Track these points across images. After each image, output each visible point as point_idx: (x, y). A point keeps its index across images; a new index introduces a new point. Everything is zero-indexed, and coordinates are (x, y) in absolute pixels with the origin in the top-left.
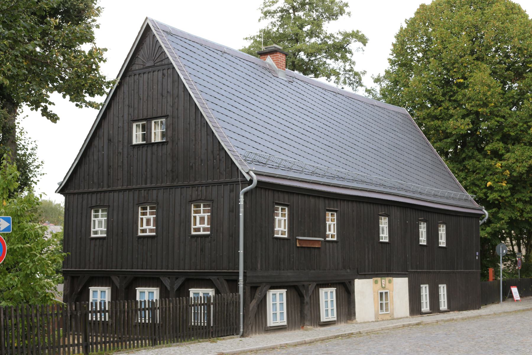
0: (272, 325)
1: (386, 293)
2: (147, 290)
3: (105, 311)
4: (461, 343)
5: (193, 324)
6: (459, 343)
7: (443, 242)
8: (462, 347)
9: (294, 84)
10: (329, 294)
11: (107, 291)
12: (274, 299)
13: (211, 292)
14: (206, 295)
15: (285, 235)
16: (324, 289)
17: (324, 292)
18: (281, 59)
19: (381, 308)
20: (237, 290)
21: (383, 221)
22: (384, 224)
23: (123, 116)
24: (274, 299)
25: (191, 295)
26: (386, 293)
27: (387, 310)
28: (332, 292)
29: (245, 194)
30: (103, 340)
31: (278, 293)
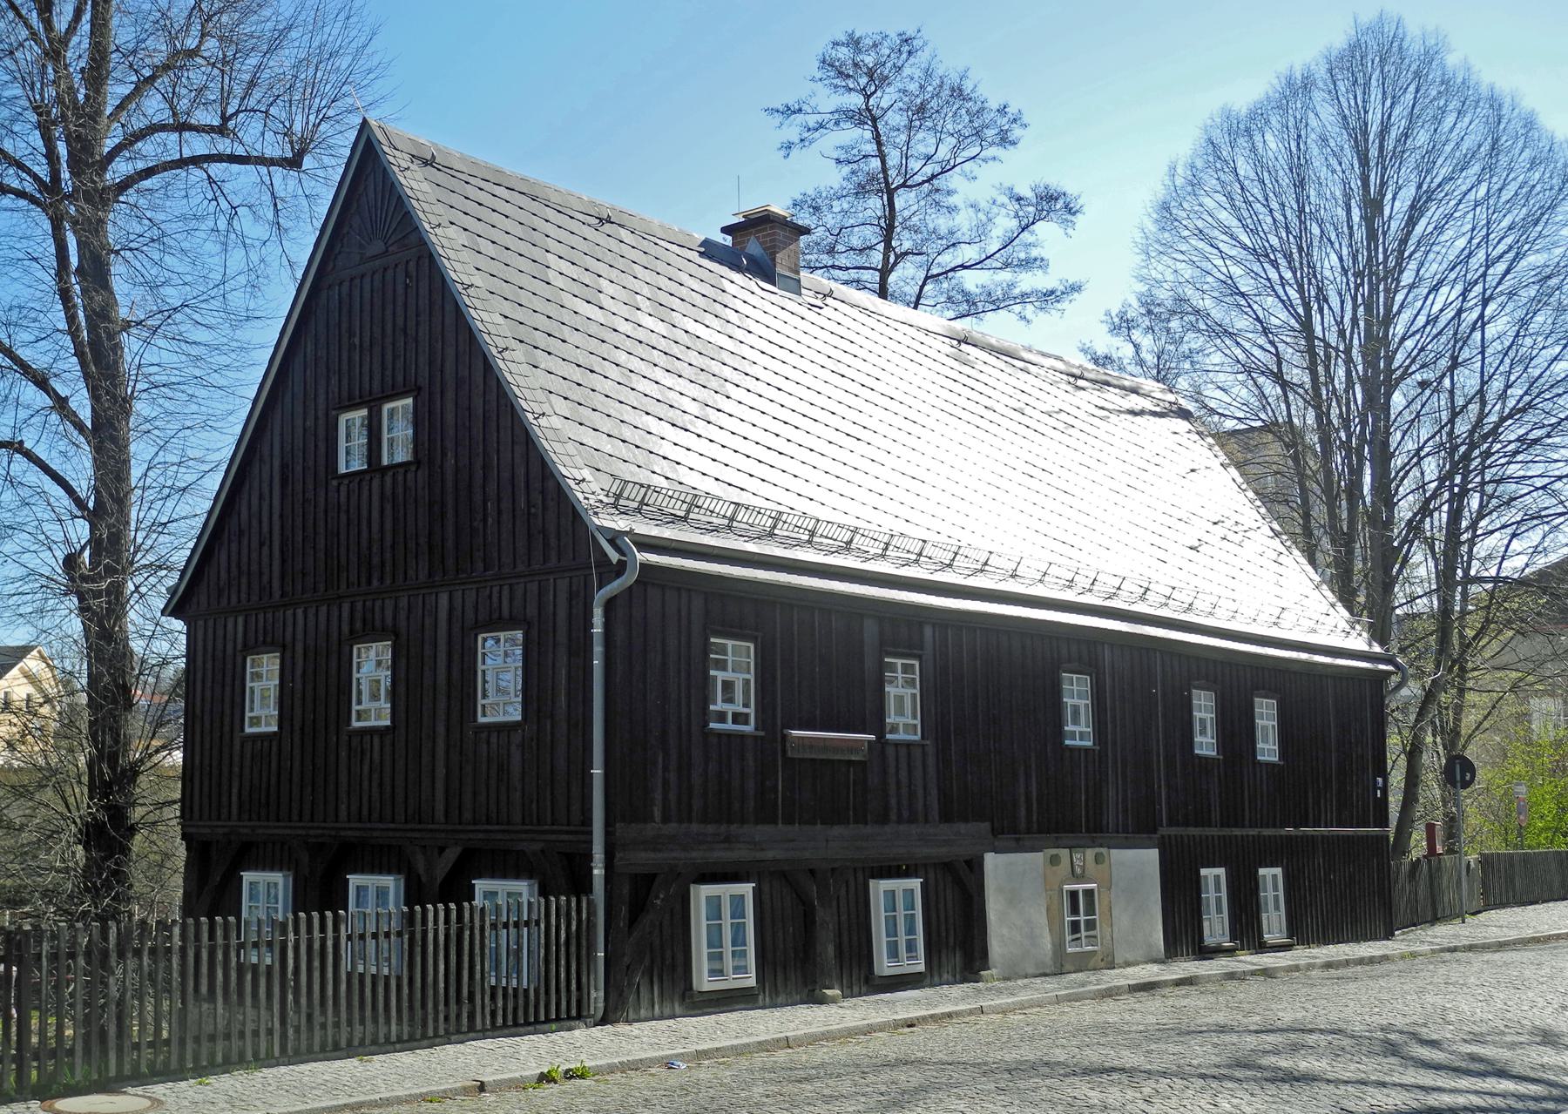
0: (887, 972)
7: (1268, 749)
9: (826, 311)
15: (746, 723)
23: (667, 478)
26: (1089, 894)
29: (609, 605)
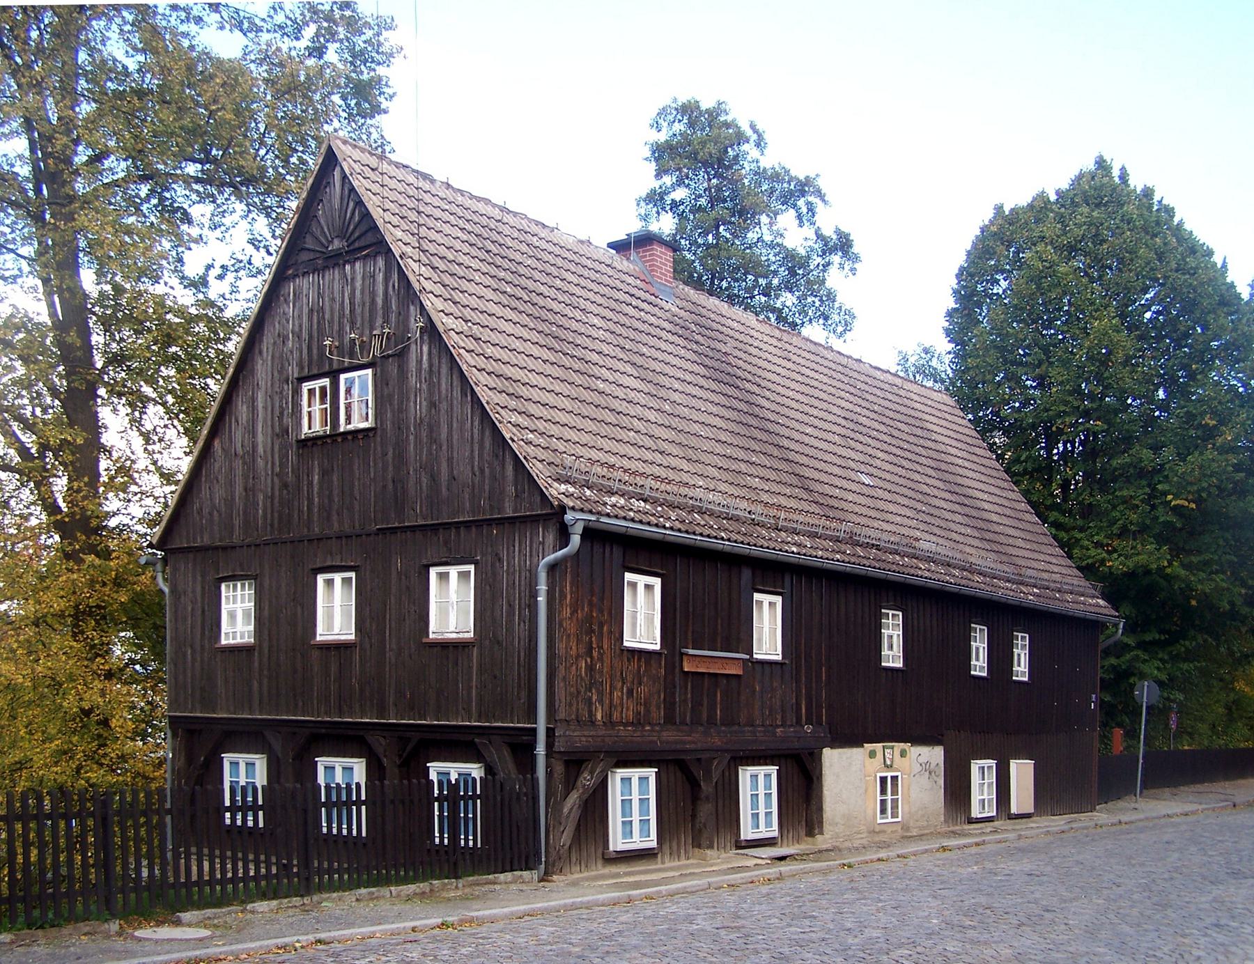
0: (620, 847)
1: (895, 778)
2: (338, 763)
3: (255, 808)
4: (1071, 900)
5: (437, 840)
6: (1065, 901)
8: (1075, 913)
10: (761, 779)
11: (356, 768)
12: (755, 785)
13: (475, 771)
14: (465, 777)
16: (749, 768)
17: (748, 774)
18: (661, 258)
19: (883, 811)
20: (533, 769)
21: (890, 621)
22: (893, 630)
24: (755, 785)
25: (433, 776)
26: (895, 778)
27: (894, 815)
28: (768, 776)
30: (263, 871)
31: (637, 776)
